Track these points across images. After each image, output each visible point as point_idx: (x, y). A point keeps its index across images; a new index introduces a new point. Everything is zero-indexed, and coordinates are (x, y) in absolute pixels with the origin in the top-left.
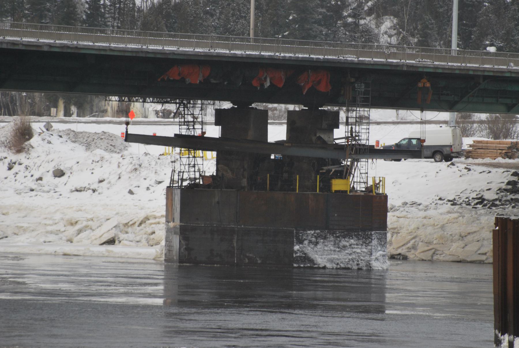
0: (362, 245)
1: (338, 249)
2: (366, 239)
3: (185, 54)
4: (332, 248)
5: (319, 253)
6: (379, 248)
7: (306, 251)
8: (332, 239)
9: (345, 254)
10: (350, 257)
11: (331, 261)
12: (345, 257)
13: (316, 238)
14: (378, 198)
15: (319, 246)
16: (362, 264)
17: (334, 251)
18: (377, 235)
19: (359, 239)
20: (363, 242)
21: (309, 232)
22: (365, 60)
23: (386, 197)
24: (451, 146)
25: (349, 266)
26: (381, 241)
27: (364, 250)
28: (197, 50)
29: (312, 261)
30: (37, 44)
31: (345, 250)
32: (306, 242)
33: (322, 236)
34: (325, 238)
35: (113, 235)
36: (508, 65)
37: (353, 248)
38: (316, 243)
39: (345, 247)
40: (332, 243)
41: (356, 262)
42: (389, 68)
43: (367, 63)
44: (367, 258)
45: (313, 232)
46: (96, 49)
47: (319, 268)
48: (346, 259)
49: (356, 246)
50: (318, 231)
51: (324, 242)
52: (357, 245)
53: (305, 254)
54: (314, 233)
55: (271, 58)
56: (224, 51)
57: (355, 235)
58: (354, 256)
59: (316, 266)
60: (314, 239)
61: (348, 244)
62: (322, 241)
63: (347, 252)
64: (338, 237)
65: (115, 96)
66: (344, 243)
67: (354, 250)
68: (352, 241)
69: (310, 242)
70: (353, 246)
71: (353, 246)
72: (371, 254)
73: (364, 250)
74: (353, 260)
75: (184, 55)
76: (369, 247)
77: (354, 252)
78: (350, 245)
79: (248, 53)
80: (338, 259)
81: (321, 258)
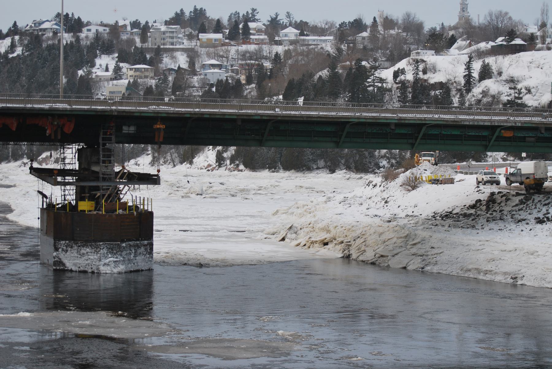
0: (94, 253)
1: (79, 256)
2: (97, 248)
3: (290, 116)
4: (76, 255)
5: (68, 259)
6: (110, 256)
7: (61, 257)
8: (76, 248)
9: (410, 246)
10: (87, 262)
11: (75, 265)
12: (84, 262)
13: (66, 247)
14: (107, 216)
15: (68, 253)
16: (94, 268)
17: (77, 257)
18: (107, 245)
19: (92, 249)
20: (95, 251)
21: (62, 242)
22: (291, 114)
23: (151, 214)
24: (534, 174)
25: (86, 269)
26: (112, 250)
27: (96, 257)
28: (8, 105)
29: (64, 265)
30: (90, 110)
31: (84, 257)
32: (60, 250)
33: (69, 245)
34: (72, 247)
35: (536, 225)
36: (274, 110)
37: (89, 255)
38: (66, 251)
39: (83, 254)
40: (76, 251)
41: (90, 266)
42: (177, 116)
43: (61, 109)
44: (97, 263)
45: (64, 242)
46: (266, 116)
47: (67, 270)
48: (84, 264)
49: (90, 254)
50: (67, 242)
51: (71, 250)
52: (91, 253)
53: (60, 259)
54: (65, 243)
55: (51, 110)
56: (234, 111)
57: (90, 245)
58: (89, 262)
59: (66, 268)
60: (65, 248)
61: (85, 252)
62: (70, 249)
63: (84, 258)
64: (79, 246)
65: (11, 142)
66: (83, 251)
67: (89, 257)
68: (88, 249)
69: (63, 250)
70: (89, 254)
71: (89, 254)
72: (100, 260)
73: (96, 257)
74: (88, 264)
75: (326, 118)
76: (99, 255)
77: (89, 258)
78: (87, 253)
79: (177, 109)
80: (79, 264)
81: (69, 263)
